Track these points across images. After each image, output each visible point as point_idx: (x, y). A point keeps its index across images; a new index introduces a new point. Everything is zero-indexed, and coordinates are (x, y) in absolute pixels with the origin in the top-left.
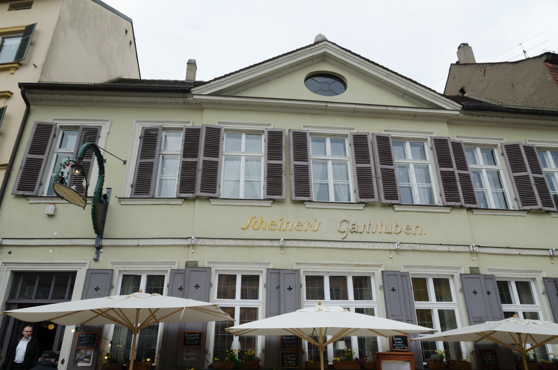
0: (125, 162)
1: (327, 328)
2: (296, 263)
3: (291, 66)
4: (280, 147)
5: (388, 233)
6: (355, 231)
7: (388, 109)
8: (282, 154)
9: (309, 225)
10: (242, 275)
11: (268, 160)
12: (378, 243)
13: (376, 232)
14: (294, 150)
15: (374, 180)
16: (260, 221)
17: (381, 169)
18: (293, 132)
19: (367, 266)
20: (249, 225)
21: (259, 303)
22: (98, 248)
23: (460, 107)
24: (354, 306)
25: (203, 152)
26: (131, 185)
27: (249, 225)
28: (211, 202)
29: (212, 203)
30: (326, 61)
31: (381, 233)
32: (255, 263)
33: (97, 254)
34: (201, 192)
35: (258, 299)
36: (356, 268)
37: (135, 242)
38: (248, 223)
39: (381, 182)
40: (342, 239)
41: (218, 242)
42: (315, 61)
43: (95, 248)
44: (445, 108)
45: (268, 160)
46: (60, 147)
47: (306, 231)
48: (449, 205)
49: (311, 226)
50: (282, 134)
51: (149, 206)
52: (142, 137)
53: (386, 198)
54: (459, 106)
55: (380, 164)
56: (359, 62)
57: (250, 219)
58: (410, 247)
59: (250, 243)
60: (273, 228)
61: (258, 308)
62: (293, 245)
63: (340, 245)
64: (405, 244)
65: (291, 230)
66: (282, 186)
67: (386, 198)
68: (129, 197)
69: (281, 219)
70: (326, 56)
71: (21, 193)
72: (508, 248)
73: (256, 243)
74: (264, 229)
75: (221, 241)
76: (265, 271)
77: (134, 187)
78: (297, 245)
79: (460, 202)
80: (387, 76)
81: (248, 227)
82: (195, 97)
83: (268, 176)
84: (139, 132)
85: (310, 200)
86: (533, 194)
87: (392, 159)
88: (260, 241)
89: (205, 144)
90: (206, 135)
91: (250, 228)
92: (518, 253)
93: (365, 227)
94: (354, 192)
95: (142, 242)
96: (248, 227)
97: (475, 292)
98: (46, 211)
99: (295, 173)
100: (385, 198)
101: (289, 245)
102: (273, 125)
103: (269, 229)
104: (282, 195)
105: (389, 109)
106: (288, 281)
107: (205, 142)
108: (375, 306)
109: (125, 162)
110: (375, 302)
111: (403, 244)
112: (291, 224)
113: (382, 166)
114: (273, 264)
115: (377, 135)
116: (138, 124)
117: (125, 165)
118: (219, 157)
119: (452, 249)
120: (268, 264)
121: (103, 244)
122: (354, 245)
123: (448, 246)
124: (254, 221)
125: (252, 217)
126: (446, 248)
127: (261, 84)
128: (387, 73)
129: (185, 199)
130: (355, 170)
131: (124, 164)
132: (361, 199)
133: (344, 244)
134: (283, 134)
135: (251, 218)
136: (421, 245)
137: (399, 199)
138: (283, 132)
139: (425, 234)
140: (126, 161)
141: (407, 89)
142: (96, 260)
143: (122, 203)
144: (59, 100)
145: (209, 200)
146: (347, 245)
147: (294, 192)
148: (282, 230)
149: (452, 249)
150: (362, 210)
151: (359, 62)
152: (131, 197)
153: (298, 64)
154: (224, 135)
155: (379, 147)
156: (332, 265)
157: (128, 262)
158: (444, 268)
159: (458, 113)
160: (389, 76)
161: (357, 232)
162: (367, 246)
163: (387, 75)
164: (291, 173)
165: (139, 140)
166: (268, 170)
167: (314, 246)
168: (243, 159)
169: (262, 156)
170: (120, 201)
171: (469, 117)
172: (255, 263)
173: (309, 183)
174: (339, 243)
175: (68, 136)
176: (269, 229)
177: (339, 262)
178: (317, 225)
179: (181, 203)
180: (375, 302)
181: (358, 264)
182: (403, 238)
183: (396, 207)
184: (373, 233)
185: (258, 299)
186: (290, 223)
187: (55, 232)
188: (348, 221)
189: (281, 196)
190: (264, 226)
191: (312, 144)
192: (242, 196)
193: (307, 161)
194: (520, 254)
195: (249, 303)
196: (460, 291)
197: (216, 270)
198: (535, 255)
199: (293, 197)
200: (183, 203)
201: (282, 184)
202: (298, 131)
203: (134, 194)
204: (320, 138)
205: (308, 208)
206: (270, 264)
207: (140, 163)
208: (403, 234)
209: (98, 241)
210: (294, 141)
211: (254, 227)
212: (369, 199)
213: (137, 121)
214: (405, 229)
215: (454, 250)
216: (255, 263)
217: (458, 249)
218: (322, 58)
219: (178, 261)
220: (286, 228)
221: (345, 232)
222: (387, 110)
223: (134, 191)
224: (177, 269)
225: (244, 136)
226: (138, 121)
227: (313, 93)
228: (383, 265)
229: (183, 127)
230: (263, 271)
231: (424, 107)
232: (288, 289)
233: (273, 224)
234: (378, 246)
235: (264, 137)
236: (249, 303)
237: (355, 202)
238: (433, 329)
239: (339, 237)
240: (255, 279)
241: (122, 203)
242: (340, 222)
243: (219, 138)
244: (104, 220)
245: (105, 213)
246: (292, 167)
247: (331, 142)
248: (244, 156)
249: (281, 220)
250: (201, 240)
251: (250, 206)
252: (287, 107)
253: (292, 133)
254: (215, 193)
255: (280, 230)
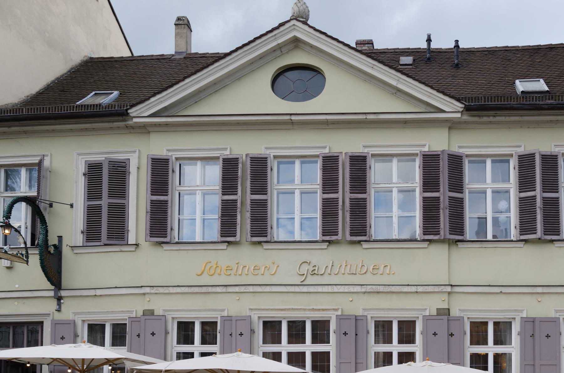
0: (72, 206)
1: (367, 369)
2: (249, 309)
3: (252, 62)
4: (236, 178)
5: (353, 274)
6: (315, 273)
7: (367, 118)
8: (237, 187)
9: (266, 268)
10: (494, 322)
11: (223, 195)
12: (337, 286)
13: (339, 274)
14: (251, 182)
15: (340, 213)
16: (215, 266)
17: (350, 199)
18: (251, 158)
19: (323, 310)
20: (204, 270)
21: (417, 348)
22: (59, 299)
23: (462, 108)
24: (397, 350)
25: (151, 190)
26: (82, 231)
27: (204, 270)
28: (263, 246)
29: (265, 247)
30: (301, 47)
31: (344, 274)
32: (209, 310)
33: (59, 305)
34: (150, 237)
35: (416, 344)
36: (312, 312)
37: (92, 293)
38: (203, 269)
39: (348, 215)
40: (301, 282)
41: (172, 290)
42: (284, 50)
43: (56, 300)
44: (444, 111)
45: (223, 195)
46: (278, 182)
47: (263, 275)
48: (426, 239)
49: (269, 268)
50: (238, 161)
51: (501, 248)
52: (86, 174)
53: (352, 234)
54: (459, 106)
55: (349, 193)
56: (337, 49)
57: (204, 265)
58: (372, 289)
59: (204, 290)
60: (229, 273)
61: (416, 352)
62: (248, 291)
63: (297, 289)
64: (368, 286)
65: (247, 275)
66: (236, 226)
67: (352, 234)
68: (81, 245)
69: (237, 263)
70: (300, 41)
71: (327, 238)
72: (489, 286)
73: (210, 289)
74: (220, 275)
75: (175, 288)
76: (421, 318)
77: (84, 233)
78: (251, 290)
79: (439, 235)
80: (373, 68)
81: (203, 273)
82: (135, 120)
83: (222, 215)
84: (82, 169)
85: (268, 241)
86: (535, 220)
87: (462, 185)
88: (214, 287)
89: (152, 180)
90: (152, 168)
91: (205, 273)
92: (499, 291)
93: (327, 268)
94: (515, 228)
95: (99, 292)
96: (203, 273)
97: (153, 334)
98: (3, 264)
99: (251, 210)
100: (350, 235)
101: (154, 291)
102: (429, 145)
103: (225, 274)
104: (236, 237)
105: (293, 118)
106: (243, 327)
107: (152, 178)
108: (417, 350)
109: (72, 206)
110: (417, 346)
111: (365, 286)
112: (247, 268)
113: (352, 195)
114: (429, 310)
115: (351, 154)
116: (80, 157)
117: (72, 208)
118: (268, 194)
119: (420, 289)
120: (223, 310)
121: (62, 295)
122: (312, 289)
123: (416, 286)
124: (208, 267)
125: (207, 262)
126: (414, 289)
127: (216, 91)
128: (372, 64)
129: (430, 241)
130: (149, 204)
131: (71, 208)
132: (352, 237)
133: (301, 287)
134: (239, 161)
135: (206, 263)
136: (386, 286)
137: (367, 236)
138: (240, 158)
139: (393, 274)
140: (73, 204)
141: (397, 84)
142: (59, 310)
143: (76, 251)
144: (110, 128)
145: (360, 243)
146: (305, 289)
147: (250, 232)
148: (238, 275)
149: (420, 289)
150: (326, 249)
151: (337, 49)
152: (84, 245)
153: (261, 57)
154: (371, 162)
155: (351, 170)
156: (274, 310)
157: (89, 312)
158: (407, 310)
159: (459, 115)
160: (374, 67)
161: (318, 275)
162: (326, 289)
163: (373, 66)
164: (247, 210)
165: (83, 177)
166: (222, 208)
167: (269, 291)
168: (297, 194)
169: (417, 187)
170: (73, 250)
171: (476, 119)
172: (210, 310)
173: (267, 221)
174: (296, 287)
175: (184, 167)
176: (225, 274)
177: (294, 307)
178: (275, 268)
179: (522, 246)
180: (417, 346)
181: (313, 309)
182: (368, 279)
183: (165, 246)
184: (335, 274)
185: (416, 344)
186: (246, 266)
187: (17, 284)
188: (309, 262)
189: (235, 237)
190: (219, 271)
191: (469, 166)
192: (198, 239)
193: (266, 194)
194: (501, 292)
195: (406, 348)
196: (169, 333)
197: (371, 317)
198: (520, 293)
199: (248, 238)
200: (227, 247)
201: (237, 223)
202: (256, 155)
203: (86, 242)
204: (479, 160)
205: (77, 253)
206: (225, 310)
207: (88, 205)
208: (369, 275)
209: (56, 292)
210: (251, 170)
211: (210, 273)
212: (332, 237)
213: (78, 154)
214: (371, 269)
215: (422, 291)
216: (209, 310)
217: (426, 289)
218: (294, 44)
219: (135, 310)
220: (242, 273)
221: (304, 274)
222: (366, 118)
223: (85, 238)
224: (526, 317)
225: (297, 163)
226: (79, 154)
227: (281, 99)
228: (340, 309)
229: (219, 155)
230: (419, 317)
231: (428, 111)
232: (344, 334)
233: (229, 268)
234: (262, 289)
235: (418, 162)
236: (406, 348)
237: (516, 240)
238: (305, 370)
239: (298, 280)
240: (412, 324)
241: (76, 251)
242: (300, 264)
243: (168, 171)
244: (59, 271)
245: (60, 263)
246: (248, 202)
247: (492, 163)
248: (396, 187)
249: (237, 264)
250: (155, 288)
251: (205, 250)
252: (88, 129)
253: (250, 159)
254: (166, 237)
255: (236, 275)
